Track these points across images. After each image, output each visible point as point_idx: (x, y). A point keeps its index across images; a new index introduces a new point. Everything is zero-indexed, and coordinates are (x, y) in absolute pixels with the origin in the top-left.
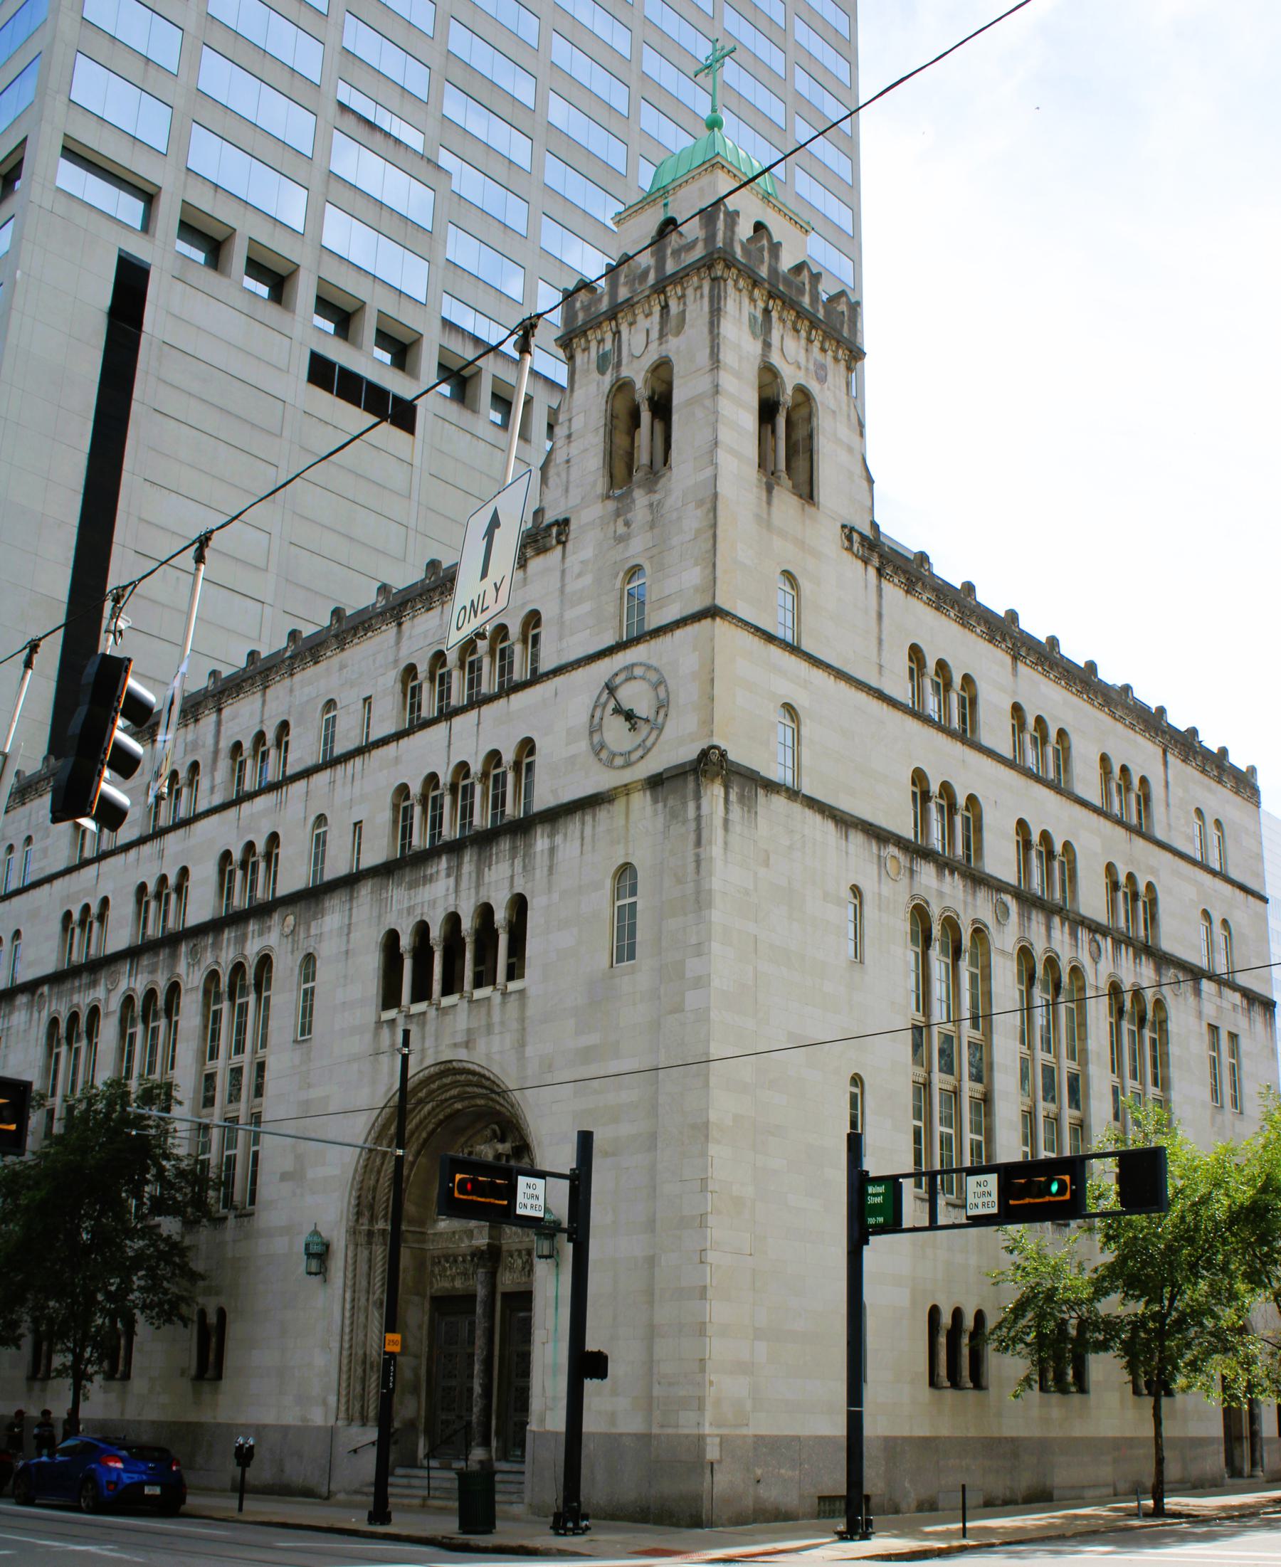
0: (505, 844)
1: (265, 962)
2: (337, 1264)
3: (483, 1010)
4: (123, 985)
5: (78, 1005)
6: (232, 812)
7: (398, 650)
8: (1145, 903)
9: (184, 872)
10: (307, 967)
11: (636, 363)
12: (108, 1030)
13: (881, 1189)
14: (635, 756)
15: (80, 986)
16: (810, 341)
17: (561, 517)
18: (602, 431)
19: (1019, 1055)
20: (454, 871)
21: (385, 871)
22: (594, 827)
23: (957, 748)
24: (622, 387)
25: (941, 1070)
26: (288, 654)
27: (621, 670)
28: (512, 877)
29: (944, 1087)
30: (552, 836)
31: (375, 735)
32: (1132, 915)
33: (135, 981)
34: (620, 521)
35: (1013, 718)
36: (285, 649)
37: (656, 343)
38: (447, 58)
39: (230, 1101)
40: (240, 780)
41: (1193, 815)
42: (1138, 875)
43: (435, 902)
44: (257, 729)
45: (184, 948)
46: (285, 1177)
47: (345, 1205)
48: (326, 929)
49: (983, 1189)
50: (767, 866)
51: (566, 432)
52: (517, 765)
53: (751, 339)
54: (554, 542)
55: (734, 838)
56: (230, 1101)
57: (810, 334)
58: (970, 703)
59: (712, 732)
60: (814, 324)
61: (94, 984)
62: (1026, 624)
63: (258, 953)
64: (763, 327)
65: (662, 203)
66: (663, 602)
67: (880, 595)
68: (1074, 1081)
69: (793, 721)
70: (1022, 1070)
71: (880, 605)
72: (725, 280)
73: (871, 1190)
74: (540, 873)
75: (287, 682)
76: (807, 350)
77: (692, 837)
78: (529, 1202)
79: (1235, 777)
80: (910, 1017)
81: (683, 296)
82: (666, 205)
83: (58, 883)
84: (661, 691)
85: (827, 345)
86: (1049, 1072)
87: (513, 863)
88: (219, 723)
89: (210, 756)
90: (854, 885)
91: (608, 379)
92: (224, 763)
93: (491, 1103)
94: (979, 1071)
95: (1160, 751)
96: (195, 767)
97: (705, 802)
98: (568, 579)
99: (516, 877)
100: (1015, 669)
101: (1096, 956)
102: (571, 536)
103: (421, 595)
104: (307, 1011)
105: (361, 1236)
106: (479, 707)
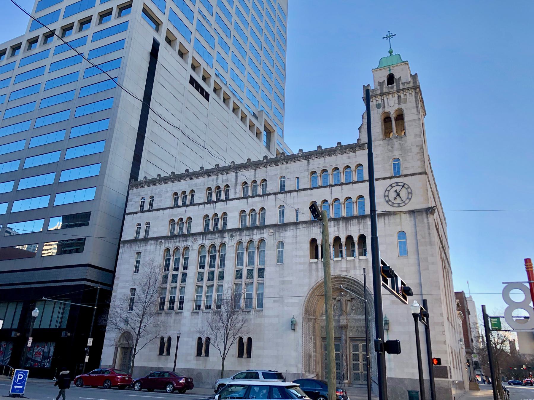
2: (299, 328)
66: (407, 168)
77: (427, 227)
87: (359, 226)
99: (361, 230)
105: (307, 320)
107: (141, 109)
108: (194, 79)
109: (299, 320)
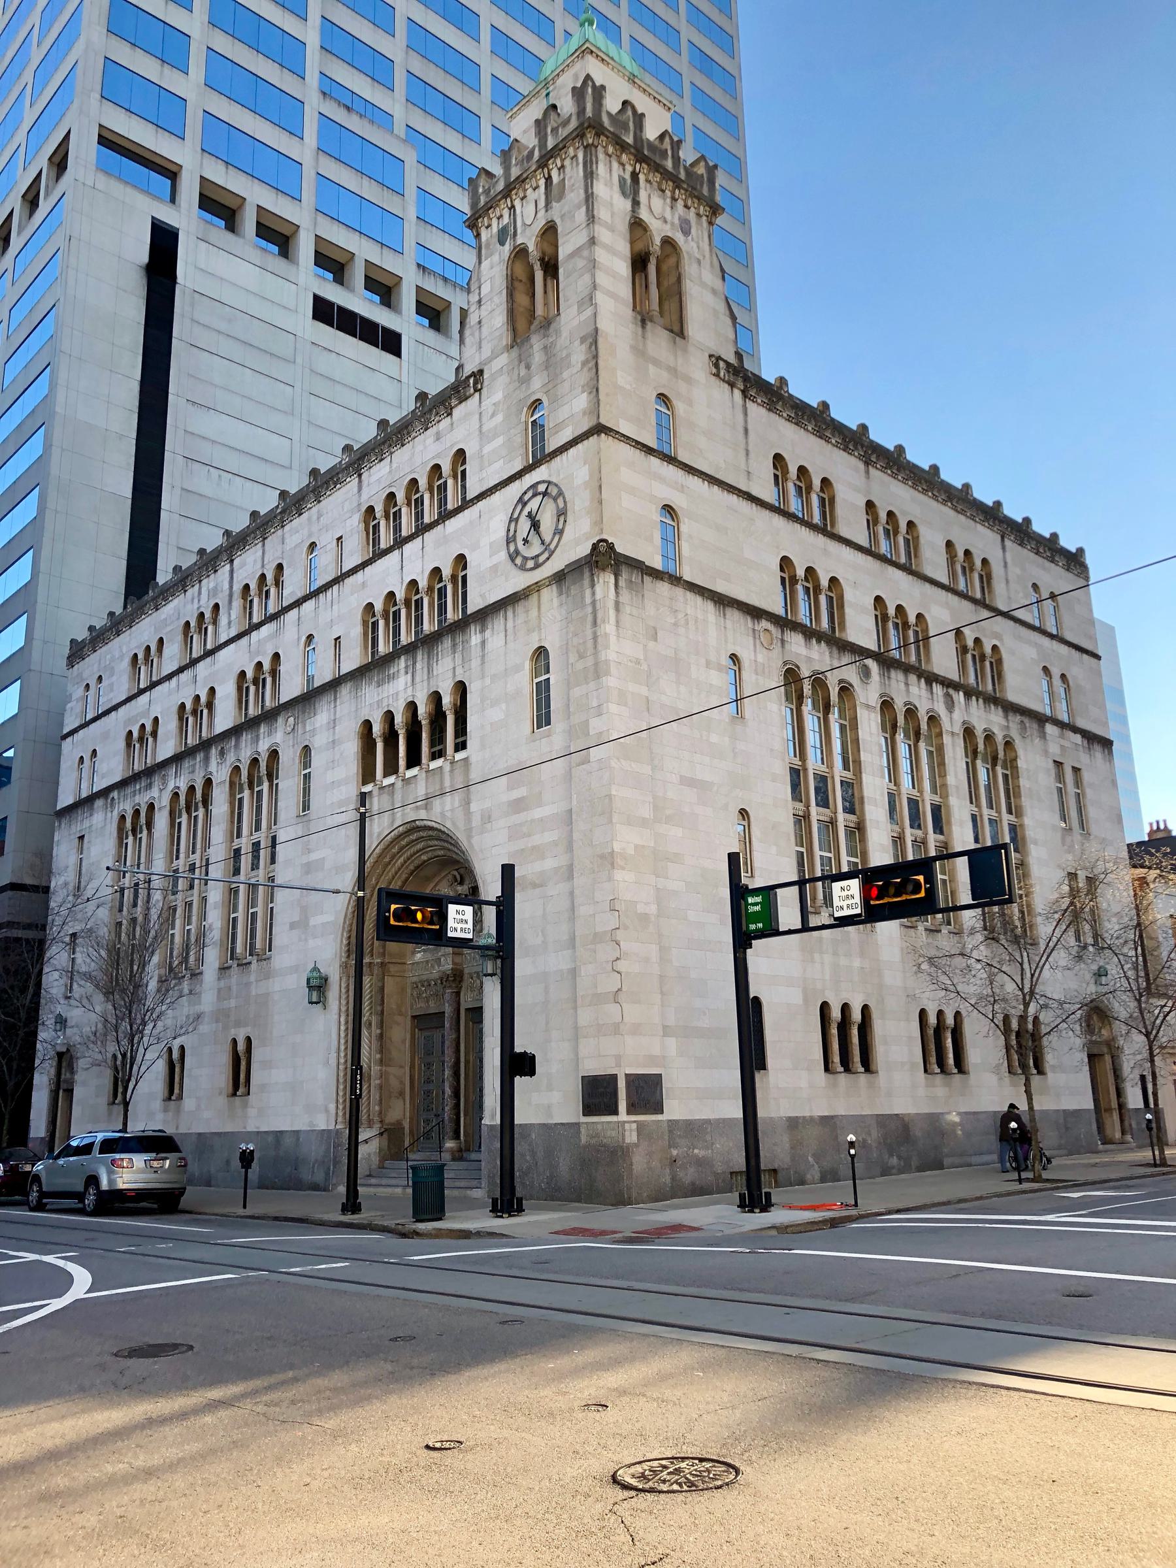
0: (447, 643)
1: (274, 754)
3: (437, 777)
4: (171, 786)
5: (139, 805)
6: (244, 641)
7: (360, 496)
8: (991, 663)
9: (212, 690)
10: (305, 757)
11: (528, 230)
12: (161, 821)
13: (759, 899)
14: (541, 559)
15: (140, 789)
16: (674, 199)
17: (475, 370)
18: (505, 292)
19: (886, 791)
20: (411, 669)
21: (359, 674)
22: (514, 621)
23: (821, 540)
24: (520, 253)
25: (817, 805)
26: (279, 511)
27: (528, 489)
28: (454, 668)
29: (822, 818)
30: (482, 631)
31: (348, 566)
32: (980, 674)
33: (179, 781)
34: (523, 365)
35: (867, 514)
36: (277, 507)
37: (543, 211)
38: (407, 53)
39: (253, 869)
40: (250, 618)
41: (1031, 590)
42: (984, 640)
43: (397, 694)
44: (260, 573)
45: (214, 752)
46: (293, 926)
47: (338, 946)
48: (318, 725)
49: (846, 893)
50: (656, 640)
51: (477, 298)
52: (454, 578)
53: (622, 198)
54: (472, 390)
55: (626, 619)
56: (253, 869)
57: (674, 193)
58: (828, 504)
59: (602, 530)
60: (677, 183)
61: (149, 786)
62: (875, 435)
63: (268, 750)
64: (631, 189)
65: (544, 94)
66: (559, 427)
67: (746, 414)
68: (937, 810)
69: (673, 520)
70: (889, 803)
71: (746, 422)
72: (596, 147)
73: (750, 900)
74: (475, 663)
75: (280, 532)
76: (672, 208)
77: (590, 618)
78: (459, 926)
79: (1065, 556)
80: (787, 761)
81: (563, 166)
82: (548, 95)
83: (122, 710)
84: (560, 501)
85: (689, 203)
86: (914, 804)
88: (232, 572)
89: (227, 598)
90: (732, 654)
91: (507, 248)
92: (237, 603)
93: (449, 854)
94: (852, 804)
95: (999, 538)
96: (216, 607)
97: (599, 589)
98: (484, 419)
100: (867, 472)
101: (950, 705)
102: (485, 384)
103: (373, 449)
104: (306, 791)
106: (423, 534)
107: (134, 435)
108: (331, 304)
109: (334, 972)
